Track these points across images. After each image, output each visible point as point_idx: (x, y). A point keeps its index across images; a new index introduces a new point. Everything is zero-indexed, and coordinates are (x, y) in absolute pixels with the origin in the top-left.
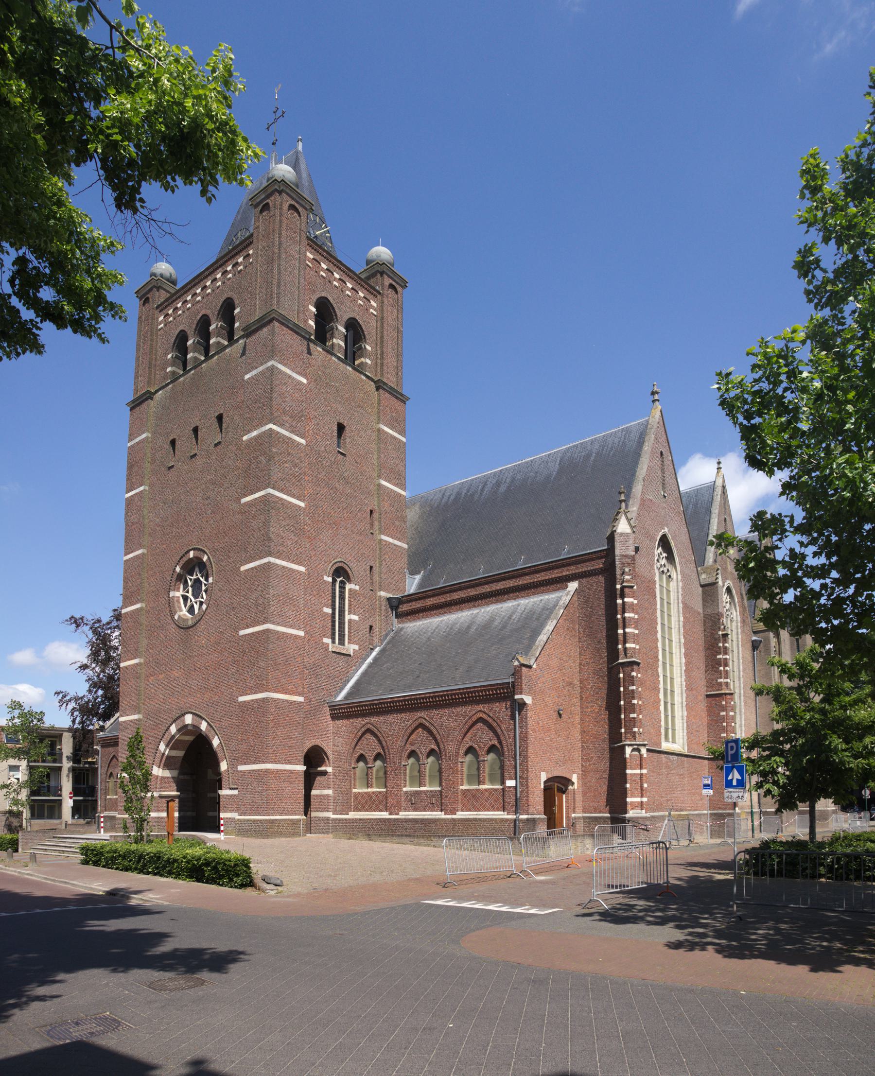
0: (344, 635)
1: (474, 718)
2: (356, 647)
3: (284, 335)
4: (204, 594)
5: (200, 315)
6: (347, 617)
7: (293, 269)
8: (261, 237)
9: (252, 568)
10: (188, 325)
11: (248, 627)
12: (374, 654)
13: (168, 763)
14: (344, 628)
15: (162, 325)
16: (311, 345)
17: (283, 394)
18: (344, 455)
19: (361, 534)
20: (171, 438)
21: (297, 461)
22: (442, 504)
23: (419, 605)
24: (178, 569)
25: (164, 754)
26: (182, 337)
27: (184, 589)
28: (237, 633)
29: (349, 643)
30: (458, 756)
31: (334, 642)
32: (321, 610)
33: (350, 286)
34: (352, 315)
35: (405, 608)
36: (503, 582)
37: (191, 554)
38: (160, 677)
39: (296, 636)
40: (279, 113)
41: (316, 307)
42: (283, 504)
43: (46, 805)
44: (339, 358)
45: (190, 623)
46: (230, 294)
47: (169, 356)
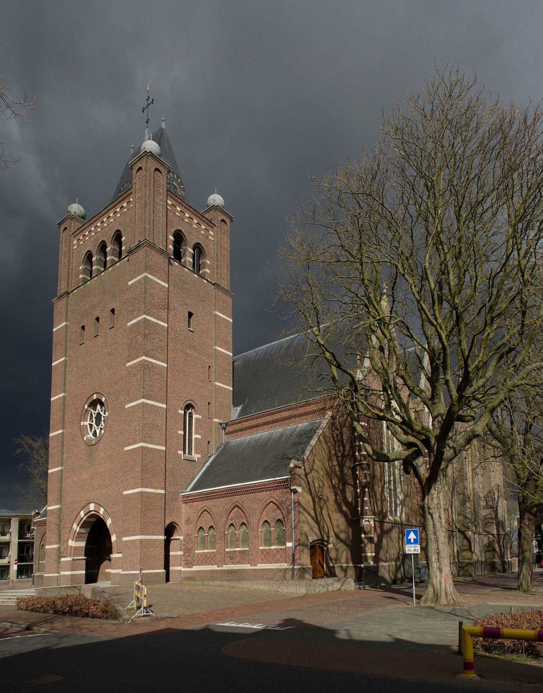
2: (199, 456)
3: (153, 256)
4: (102, 422)
5: (100, 241)
6: (194, 436)
7: (158, 212)
8: (137, 190)
9: (132, 406)
12: (211, 460)
14: (192, 444)
15: (76, 247)
18: (193, 332)
19: (203, 382)
20: (82, 325)
21: (162, 338)
23: (238, 427)
24: (86, 407)
25: (76, 531)
26: (89, 256)
27: (90, 420)
28: (123, 449)
29: (195, 453)
31: (185, 453)
32: (177, 432)
33: (196, 221)
35: (229, 429)
37: (95, 397)
38: (74, 479)
39: (160, 450)
41: (174, 236)
42: (152, 366)
45: (94, 442)
46: (119, 228)
47: (81, 268)
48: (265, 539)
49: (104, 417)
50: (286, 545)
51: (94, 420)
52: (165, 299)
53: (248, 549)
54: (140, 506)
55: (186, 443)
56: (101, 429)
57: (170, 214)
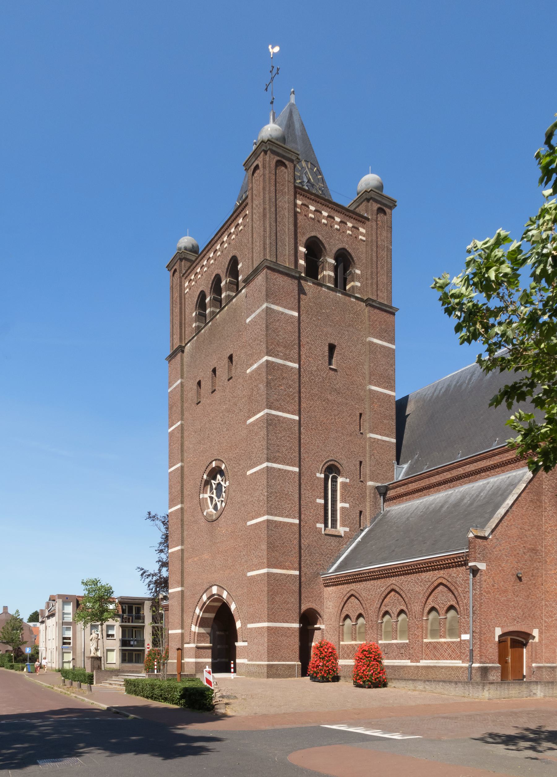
0: (336, 521)
1: (436, 584)
2: (347, 529)
3: (275, 279)
4: (224, 494)
5: (214, 275)
6: (339, 505)
7: (283, 218)
9: (255, 473)
10: (205, 285)
11: (253, 519)
12: (363, 533)
13: (202, 623)
16: (302, 282)
17: (277, 329)
19: (351, 435)
21: (290, 383)
22: (434, 398)
23: (403, 491)
24: (205, 477)
25: (199, 616)
26: (202, 296)
27: (211, 491)
30: (423, 615)
31: (326, 526)
34: (340, 246)
36: (475, 464)
37: (214, 464)
38: (195, 559)
40: (275, 71)
41: (306, 247)
42: (279, 420)
43: (134, 653)
44: (329, 288)
45: (214, 517)
47: (194, 314)
48: (431, 630)
49: (225, 487)
50: (460, 637)
51: (215, 491)
52: (295, 332)
53: (407, 641)
54: (266, 589)
55: (327, 515)
56: (222, 501)
57: (300, 217)
